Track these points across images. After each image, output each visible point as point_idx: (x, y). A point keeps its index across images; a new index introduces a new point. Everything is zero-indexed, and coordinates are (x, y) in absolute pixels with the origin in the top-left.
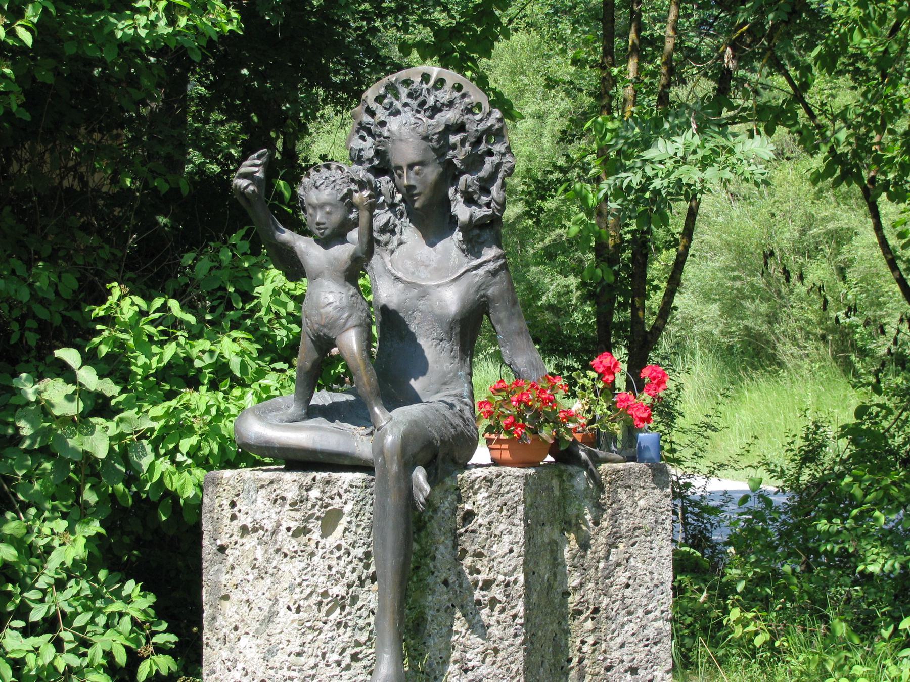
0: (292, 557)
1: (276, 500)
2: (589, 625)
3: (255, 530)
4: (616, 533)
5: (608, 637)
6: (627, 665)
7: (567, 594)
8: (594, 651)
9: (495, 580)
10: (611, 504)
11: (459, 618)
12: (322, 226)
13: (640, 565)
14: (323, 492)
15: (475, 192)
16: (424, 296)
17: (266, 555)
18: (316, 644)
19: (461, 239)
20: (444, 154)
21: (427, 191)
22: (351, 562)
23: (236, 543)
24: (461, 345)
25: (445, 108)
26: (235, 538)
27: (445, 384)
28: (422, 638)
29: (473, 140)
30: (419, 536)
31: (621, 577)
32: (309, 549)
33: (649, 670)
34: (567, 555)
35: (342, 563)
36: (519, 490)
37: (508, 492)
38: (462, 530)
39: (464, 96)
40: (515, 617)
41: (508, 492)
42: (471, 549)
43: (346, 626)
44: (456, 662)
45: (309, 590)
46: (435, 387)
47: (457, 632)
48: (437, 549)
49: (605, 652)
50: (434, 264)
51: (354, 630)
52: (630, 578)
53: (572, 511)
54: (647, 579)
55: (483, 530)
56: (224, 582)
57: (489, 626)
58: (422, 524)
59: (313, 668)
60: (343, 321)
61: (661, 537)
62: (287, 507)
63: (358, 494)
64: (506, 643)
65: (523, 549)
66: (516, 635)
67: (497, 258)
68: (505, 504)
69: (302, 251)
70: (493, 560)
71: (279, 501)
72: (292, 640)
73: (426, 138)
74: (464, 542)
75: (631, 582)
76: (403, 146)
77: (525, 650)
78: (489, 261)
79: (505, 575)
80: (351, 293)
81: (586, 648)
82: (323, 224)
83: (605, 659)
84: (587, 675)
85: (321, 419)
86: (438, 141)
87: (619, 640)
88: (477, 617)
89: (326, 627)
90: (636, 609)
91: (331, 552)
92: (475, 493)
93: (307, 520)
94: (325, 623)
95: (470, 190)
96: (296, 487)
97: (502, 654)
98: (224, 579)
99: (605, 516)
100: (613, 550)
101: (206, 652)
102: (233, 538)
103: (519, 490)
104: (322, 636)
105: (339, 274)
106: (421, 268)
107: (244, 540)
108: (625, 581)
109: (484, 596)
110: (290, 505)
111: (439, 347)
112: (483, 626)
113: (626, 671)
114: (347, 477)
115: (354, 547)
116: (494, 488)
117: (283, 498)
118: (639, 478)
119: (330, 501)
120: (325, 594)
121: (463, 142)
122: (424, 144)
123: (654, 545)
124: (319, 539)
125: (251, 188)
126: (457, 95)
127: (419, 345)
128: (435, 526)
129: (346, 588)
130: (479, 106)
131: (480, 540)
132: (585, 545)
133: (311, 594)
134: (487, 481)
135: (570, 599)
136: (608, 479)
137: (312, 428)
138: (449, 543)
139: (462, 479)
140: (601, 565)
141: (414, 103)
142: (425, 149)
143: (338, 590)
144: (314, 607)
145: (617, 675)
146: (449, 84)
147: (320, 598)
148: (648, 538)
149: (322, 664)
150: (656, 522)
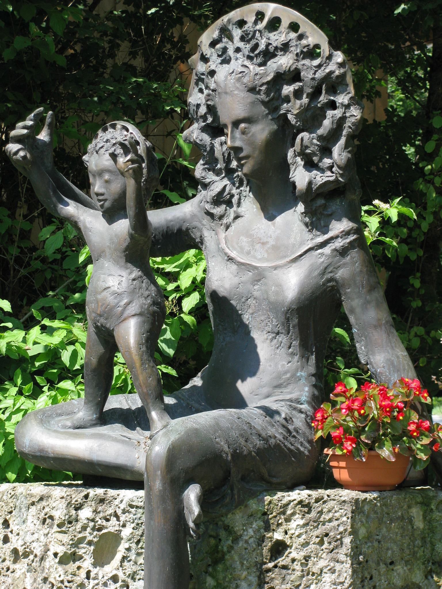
1: (44, 520)
3: (26, 555)
12: (101, 198)
14: (95, 511)
15: (314, 154)
16: (259, 280)
17: (35, 585)
19: (303, 211)
20: (277, 109)
21: (256, 153)
24: (301, 340)
25: (280, 53)
26: (7, 563)
29: (310, 90)
30: (215, 570)
36: (345, 519)
37: (330, 520)
38: (271, 565)
39: (301, 37)
41: (330, 520)
46: (265, 390)
50: (272, 242)
55: (297, 566)
58: (220, 555)
60: (120, 309)
62: (56, 528)
63: (139, 515)
67: (347, 233)
68: (327, 535)
69: (85, 227)
71: (48, 521)
73: (252, 90)
74: (272, 579)
76: (228, 99)
78: (337, 237)
80: (133, 276)
82: (102, 194)
86: (267, 93)
92: (288, 520)
93: (77, 543)
95: (308, 151)
96: (63, 505)
102: (5, 564)
103: (345, 519)
105: (119, 254)
106: (258, 246)
107: (17, 566)
110: (59, 526)
111: (275, 341)
115: (133, 579)
116: (313, 514)
117: (51, 518)
121: (298, 94)
122: (252, 97)
124: (91, 568)
125: (22, 153)
126: (293, 35)
127: (253, 339)
128: (236, 558)
131: (293, 577)
134: (303, 506)
138: (253, 579)
139: (270, 502)
141: (246, 48)
142: (253, 103)
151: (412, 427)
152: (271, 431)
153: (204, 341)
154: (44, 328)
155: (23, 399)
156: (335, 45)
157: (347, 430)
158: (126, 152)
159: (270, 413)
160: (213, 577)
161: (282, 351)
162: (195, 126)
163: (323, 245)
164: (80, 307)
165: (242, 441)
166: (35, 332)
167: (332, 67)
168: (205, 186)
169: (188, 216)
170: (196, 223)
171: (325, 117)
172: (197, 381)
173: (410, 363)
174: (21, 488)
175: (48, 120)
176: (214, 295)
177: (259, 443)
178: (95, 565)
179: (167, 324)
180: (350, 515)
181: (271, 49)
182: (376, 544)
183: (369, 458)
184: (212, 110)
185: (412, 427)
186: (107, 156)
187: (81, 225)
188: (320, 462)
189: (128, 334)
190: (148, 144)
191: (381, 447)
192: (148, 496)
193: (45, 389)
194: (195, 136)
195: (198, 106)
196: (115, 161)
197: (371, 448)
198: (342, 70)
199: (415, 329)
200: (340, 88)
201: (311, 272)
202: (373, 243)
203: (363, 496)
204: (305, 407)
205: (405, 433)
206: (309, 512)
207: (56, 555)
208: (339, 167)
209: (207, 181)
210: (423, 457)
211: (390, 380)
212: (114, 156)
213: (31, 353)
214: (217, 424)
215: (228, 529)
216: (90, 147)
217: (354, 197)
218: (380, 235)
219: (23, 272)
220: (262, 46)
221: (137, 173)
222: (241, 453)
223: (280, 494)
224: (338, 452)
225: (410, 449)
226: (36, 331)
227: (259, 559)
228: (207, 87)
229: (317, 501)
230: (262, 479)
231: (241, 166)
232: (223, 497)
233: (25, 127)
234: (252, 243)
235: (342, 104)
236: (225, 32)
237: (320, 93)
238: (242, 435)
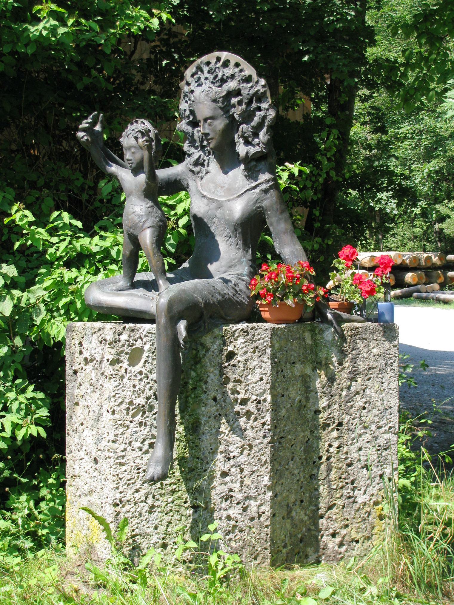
0: (110, 378)
1: (101, 341)
2: (335, 434)
3: (92, 361)
4: (355, 371)
5: (349, 443)
6: (363, 463)
7: (317, 412)
8: (338, 452)
9: (249, 399)
10: (351, 351)
11: (223, 423)
13: (373, 394)
14: (130, 336)
15: (249, 136)
18: (125, 436)
20: (228, 111)
21: (217, 137)
22: (149, 383)
23: (82, 369)
24: (243, 241)
25: (229, 80)
26: (82, 365)
27: (231, 267)
28: (198, 435)
29: (246, 101)
30: (196, 367)
31: (359, 402)
32: (120, 374)
33: (380, 468)
34: (318, 385)
35: (142, 383)
36: (267, 339)
37: (259, 340)
38: (226, 364)
39: (241, 71)
40: (264, 424)
41: (259, 340)
42: (232, 377)
43: (146, 425)
44: (222, 452)
45: (120, 400)
46: (223, 269)
47: (222, 433)
48: (208, 376)
49: (347, 453)
50: (226, 186)
51: (151, 427)
52: (365, 403)
53: (322, 355)
54: (379, 403)
55: (241, 365)
56: (76, 394)
57: (245, 430)
58: (198, 359)
59: (123, 451)
61: (389, 375)
62: (108, 346)
64: (258, 441)
65: (270, 378)
66: (264, 437)
67: (268, 181)
68: (257, 347)
69: (122, 179)
70: (248, 385)
71: (103, 342)
72: (110, 432)
73: (215, 101)
75: (366, 406)
76: (201, 106)
77: (272, 447)
78: (262, 183)
79: (257, 395)
80: (148, 205)
81: (332, 450)
82: (131, 160)
83: (346, 458)
84: (333, 469)
85: (142, 289)
86: (223, 102)
87: (358, 445)
88: (237, 423)
89: (132, 425)
90: (370, 425)
91: (135, 376)
92: (236, 340)
93: (119, 354)
94: (131, 422)
96: (111, 332)
97: (255, 449)
98: (76, 391)
99: (346, 359)
100: (354, 383)
101: (68, 439)
104: (129, 431)
106: (219, 189)
107: (87, 367)
108: (362, 404)
109: (242, 409)
110: (110, 344)
112: (241, 429)
113: (363, 467)
114: (147, 327)
115: (151, 373)
116: (250, 336)
117: (105, 340)
118: (373, 333)
119: (134, 342)
120: (131, 403)
121: (240, 103)
122: (214, 105)
123: (384, 381)
124: (127, 367)
125: (86, 138)
127: (216, 241)
128: (207, 361)
129: (145, 400)
130: (250, 77)
131: (239, 371)
132: (332, 379)
133: (122, 403)
134: (244, 332)
135: (320, 416)
136: (349, 333)
137: (128, 295)
138: (217, 372)
139: (226, 330)
140: (344, 393)
141: (211, 77)
143: (140, 401)
144: (125, 412)
145: (355, 469)
146: (232, 63)
147: (128, 406)
148: (380, 376)
149: (129, 449)
150: (386, 364)
151: (305, 288)
152: (226, 291)
153: (190, 242)
154: (101, 237)
155: (89, 276)
156: (260, 75)
157: (268, 290)
158: (143, 135)
159: (226, 281)
160: (195, 371)
161: (233, 247)
162: (184, 121)
163: (255, 187)
164: (120, 225)
165: (210, 296)
166: (96, 238)
167: (259, 87)
168: (189, 155)
169: (180, 172)
170: (184, 176)
171: (255, 116)
172: (186, 265)
173: (304, 253)
174: (89, 324)
175: (100, 119)
176: (195, 216)
177: (219, 298)
178: (129, 365)
179: (170, 234)
180: (270, 336)
181: (225, 78)
182: (285, 352)
183: (280, 305)
184: (192, 112)
185: (305, 288)
186: (133, 139)
187: (119, 178)
188: (254, 308)
189: (146, 238)
190: (156, 131)
191: (287, 298)
192: (158, 328)
193: (102, 270)
194: (183, 127)
195: (185, 110)
196: (137, 141)
197: (282, 300)
198: (264, 89)
199: (316, 239)
200: (263, 100)
201: (248, 202)
202: (286, 188)
203: (277, 326)
204: (246, 278)
205: (301, 291)
206: (247, 335)
207: (108, 360)
208: (263, 143)
209: (190, 152)
210: (310, 304)
211: (292, 262)
212: (136, 138)
213: (94, 251)
214: (196, 287)
215: (203, 345)
216: (124, 133)
217: (272, 161)
218: (290, 183)
219: (91, 208)
220: (220, 76)
221: (149, 148)
222: (209, 303)
223: (231, 326)
224: (264, 302)
225: (303, 300)
226: (97, 238)
227: (220, 361)
228: (190, 100)
229: (252, 329)
230: (221, 317)
231: (209, 144)
232: (200, 327)
233: (87, 123)
234: (216, 187)
235: (264, 108)
236: (200, 69)
237: (252, 102)
238: (209, 293)
